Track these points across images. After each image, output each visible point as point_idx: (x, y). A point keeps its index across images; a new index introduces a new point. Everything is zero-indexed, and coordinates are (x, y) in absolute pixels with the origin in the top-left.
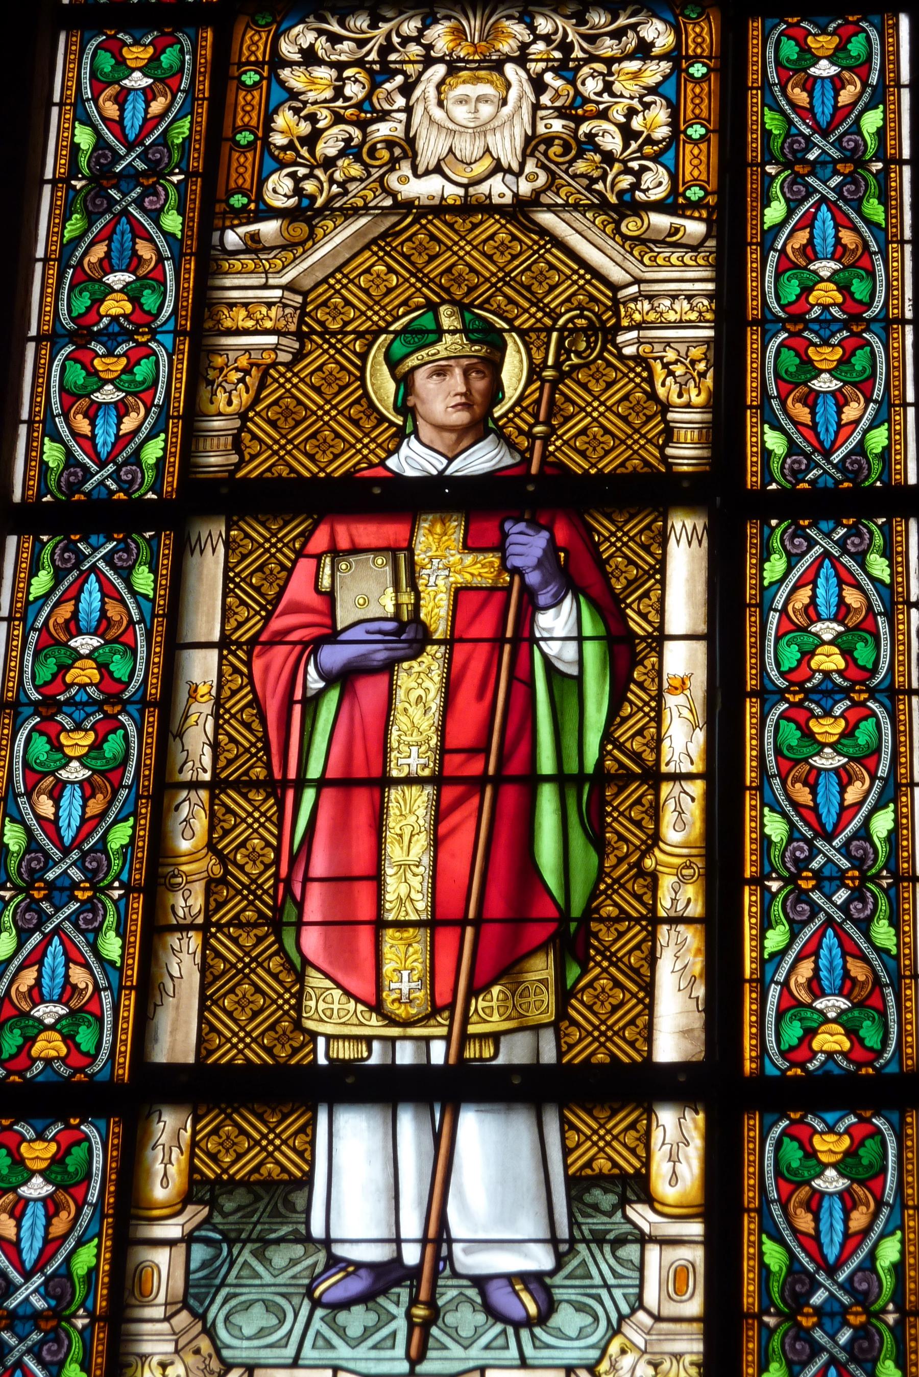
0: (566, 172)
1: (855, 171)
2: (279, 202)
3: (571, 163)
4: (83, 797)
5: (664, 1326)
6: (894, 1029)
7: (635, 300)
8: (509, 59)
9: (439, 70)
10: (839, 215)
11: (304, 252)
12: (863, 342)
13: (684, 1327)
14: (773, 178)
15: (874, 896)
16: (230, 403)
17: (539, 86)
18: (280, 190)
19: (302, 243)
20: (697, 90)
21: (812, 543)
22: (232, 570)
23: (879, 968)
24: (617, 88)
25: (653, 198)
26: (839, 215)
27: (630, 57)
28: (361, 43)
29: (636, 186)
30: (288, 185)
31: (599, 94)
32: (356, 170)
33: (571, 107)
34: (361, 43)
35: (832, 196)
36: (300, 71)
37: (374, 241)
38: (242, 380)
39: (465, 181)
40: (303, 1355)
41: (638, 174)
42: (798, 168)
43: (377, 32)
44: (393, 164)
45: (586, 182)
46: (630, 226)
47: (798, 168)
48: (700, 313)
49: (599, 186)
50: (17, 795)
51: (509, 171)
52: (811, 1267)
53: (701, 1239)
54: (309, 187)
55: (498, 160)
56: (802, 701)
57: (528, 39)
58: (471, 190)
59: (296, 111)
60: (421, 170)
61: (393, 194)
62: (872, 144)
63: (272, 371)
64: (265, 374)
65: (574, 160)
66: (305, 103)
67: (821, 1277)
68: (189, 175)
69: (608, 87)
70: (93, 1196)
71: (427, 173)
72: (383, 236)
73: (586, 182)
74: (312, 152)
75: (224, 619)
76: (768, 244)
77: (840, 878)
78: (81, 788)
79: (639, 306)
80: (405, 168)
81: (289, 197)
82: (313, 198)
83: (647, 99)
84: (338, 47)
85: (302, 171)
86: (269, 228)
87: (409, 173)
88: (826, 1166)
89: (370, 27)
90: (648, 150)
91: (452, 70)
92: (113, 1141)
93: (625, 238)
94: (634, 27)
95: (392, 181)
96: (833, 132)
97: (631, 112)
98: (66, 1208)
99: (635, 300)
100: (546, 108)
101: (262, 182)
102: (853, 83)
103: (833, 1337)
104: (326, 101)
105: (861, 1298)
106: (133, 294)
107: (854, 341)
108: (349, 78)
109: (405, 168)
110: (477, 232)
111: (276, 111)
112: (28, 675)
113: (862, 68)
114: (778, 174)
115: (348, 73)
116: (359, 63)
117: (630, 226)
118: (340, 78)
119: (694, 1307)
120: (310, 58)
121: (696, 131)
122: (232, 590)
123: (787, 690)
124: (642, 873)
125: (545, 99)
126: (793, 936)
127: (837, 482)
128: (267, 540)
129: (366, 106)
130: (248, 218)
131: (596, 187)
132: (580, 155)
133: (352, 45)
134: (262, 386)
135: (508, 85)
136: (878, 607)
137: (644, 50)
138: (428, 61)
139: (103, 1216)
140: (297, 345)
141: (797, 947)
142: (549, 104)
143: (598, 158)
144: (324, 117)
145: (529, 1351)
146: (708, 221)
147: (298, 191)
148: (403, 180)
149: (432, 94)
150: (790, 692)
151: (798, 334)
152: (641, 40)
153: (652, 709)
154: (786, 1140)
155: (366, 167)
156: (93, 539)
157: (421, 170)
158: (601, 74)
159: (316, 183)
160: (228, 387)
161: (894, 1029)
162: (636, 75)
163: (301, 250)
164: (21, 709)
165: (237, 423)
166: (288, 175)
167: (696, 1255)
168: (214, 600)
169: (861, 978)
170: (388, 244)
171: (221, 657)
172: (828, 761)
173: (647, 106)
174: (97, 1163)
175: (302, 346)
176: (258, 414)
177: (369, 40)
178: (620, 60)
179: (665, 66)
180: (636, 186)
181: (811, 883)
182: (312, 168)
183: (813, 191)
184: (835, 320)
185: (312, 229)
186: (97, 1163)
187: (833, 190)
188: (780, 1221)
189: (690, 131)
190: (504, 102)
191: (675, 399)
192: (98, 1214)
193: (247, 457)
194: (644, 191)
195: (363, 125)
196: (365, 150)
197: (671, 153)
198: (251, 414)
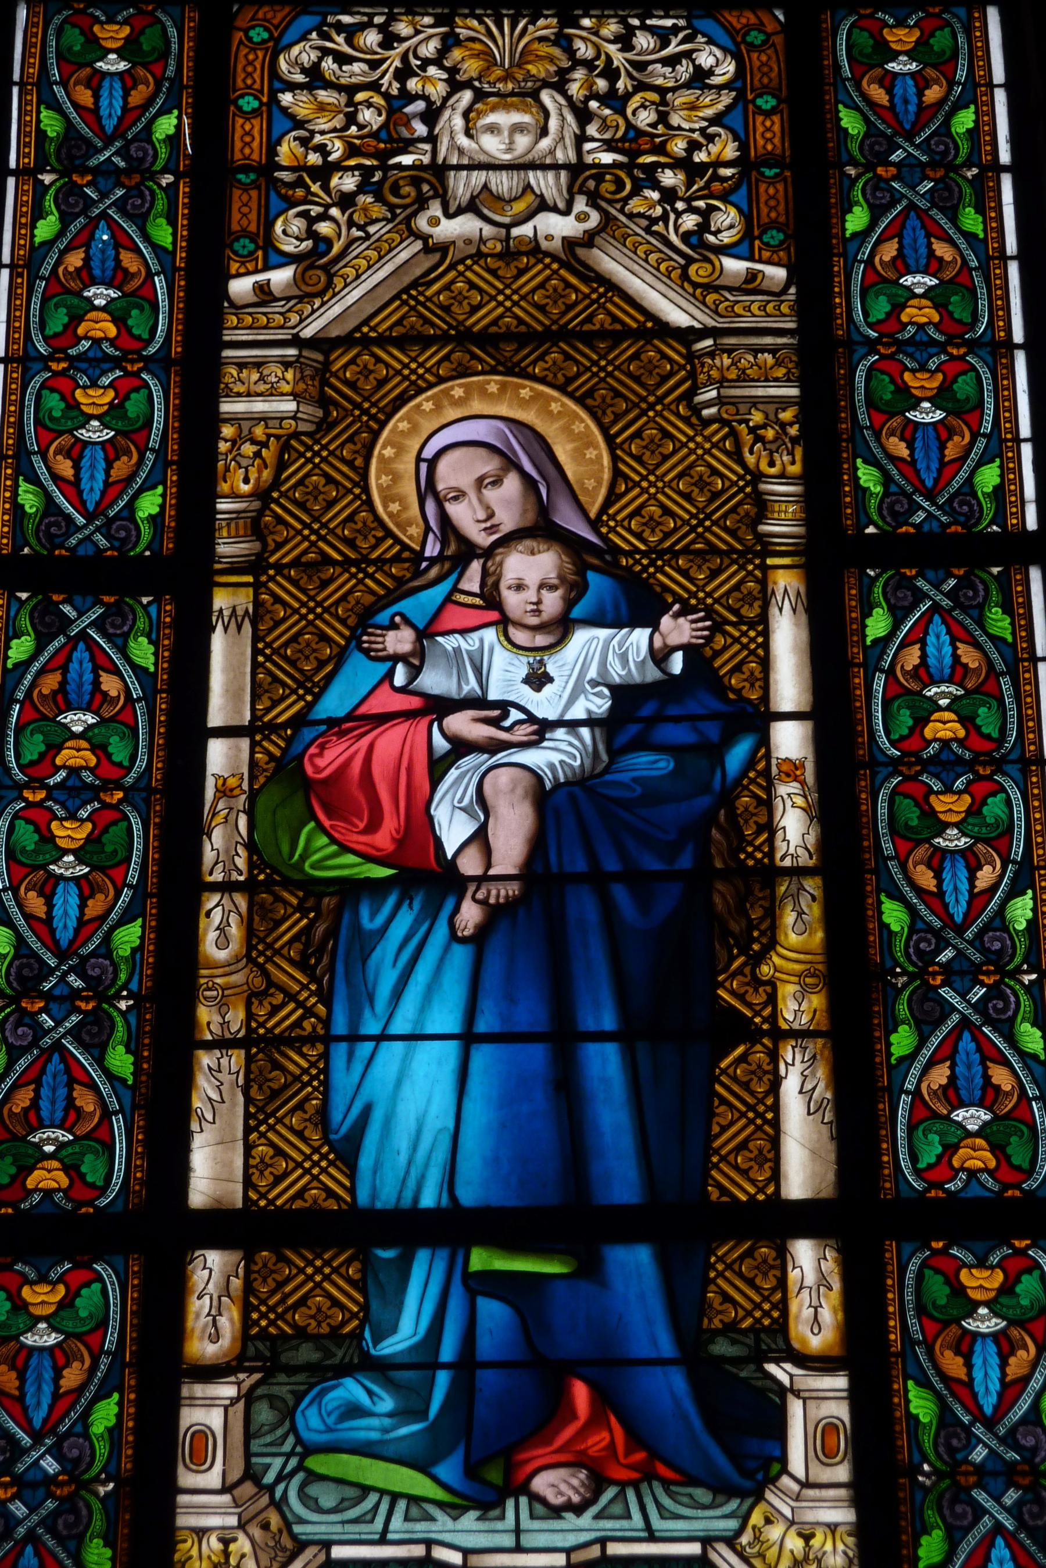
0: (622, 211)
1: (946, 175)
2: (289, 246)
3: (625, 200)
4: (106, 459)
5: (811, 1493)
6: (1013, 713)
7: (712, 355)
8: (546, 84)
9: (467, 96)
10: (956, 628)
11: (323, 304)
12: (966, 367)
13: (832, 1493)
14: (854, 181)
15: (983, 582)
16: (246, 481)
17: (583, 116)
18: (289, 231)
19: (321, 294)
20: (771, 191)
21: (922, 596)
22: (262, 639)
23: (995, 656)
24: (675, 120)
25: (726, 241)
26: (956, 628)
27: (688, 85)
28: (374, 65)
29: (704, 227)
30: (297, 226)
31: (653, 125)
32: (378, 211)
33: (623, 139)
34: (374, 65)
35: (946, 603)
36: (304, 96)
37: (406, 290)
38: (258, 454)
39: (507, 220)
40: (391, 1527)
41: (706, 214)
42: (880, 170)
43: (392, 52)
44: (421, 203)
45: (644, 223)
46: (698, 272)
47: (880, 170)
48: (769, 35)
49: (659, 228)
50: (30, 453)
51: (555, 209)
52: (966, 1419)
53: (844, 1394)
54: (324, 228)
55: (542, 196)
56: (893, 354)
57: (566, 64)
58: (516, 232)
59: (304, 142)
60: (452, 209)
61: (425, 238)
62: (964, 148)
63: (293, 442)
64: (286, 447)
65: (630, 196)
66: (312, 133)
67: (979, 1430)
68: (178, 176)
69: (663, 118)
70: (154, 440)
71: (460, 211)
72: (415, 284)
73: (644, 223)
74: (326, 188)
75: (255, 698)
76: (872, 662)
77: (974, 973)
78: (104, 449)
79: (717, 362)
80: (435, 209)
81: (302, 240)
82: (328, 242)
83: (712, 130)
84: (344, 68)
85: (315, 210)
86: (281, 277)
87: (439, 213)
88: (978, 1304)
89: (380, 45)
90: (716, 186)
91: (480, 95)
92: (174, 390)
93: (695, 285)
94: (688, 54)
95: (422, 223)
96: (918, 134)
97: (693, 146)
98: (128, 453)
99: (712, 355)
100: (593, 140)
101: (270, 225)
102: (937, 82)
103: (960, 953)
104: (334, 130)
105: (992, 957)
106: (117, 314)
107: (954, 367)
108: (360, 103)
109: (435, 209)
110: (523, 279)
111: (279, 143)
112: (34, 320)
113: (945, 64)
114: (859, 176)
115: (360, 97)
116: (374, 86)
117: (701, 272)
118: (350, 103)
119: (842, 1473)
120: (315, 78)
121: (767, 102)
122: (262, 665)
123: (878, 341)
124: (757, 982)
125: (592, 130)
126: (922, 1041)
127: (944, 526)
128: (303, 604)
129: (383, 135)
130: (253, 1116)
131: (655, 228)
132: (636, 191)
133: (364, 67)
134: (281, 466)
135: (547, 114)
136: (1000, 665)
137: (700, 77)
138: (455, 86)
139: (167, 464)
140: (320, 413)
141: (927, 1053)
142: (597, 136)
143: (655, 195)
144: (337, 150)
145: (657, 1523)
146: (788, 267)
147: (311, 234)
148: (434, 222)
149: (458, 122)
150: (904, 764)
151: (914, 778)
152: (698, 68)
153: (774, 1306)
154: (928, 1272)
155: (392, 208)
156: (90, 550)
157: (452, 209)
158: (653, 103)
159: (334, 226)
160: (244, 462)
161: (1013, 713)
162: (693, 107)
163: (317, 303)
164: (29, 364)
165: (256, 505)
166: (299, 215)
167: (841, 1411)
168: (243, 702)
169: (973, 665)
170: (421, 293)
171: (253, 745)
172: (953, 840)
173: (711, 138)
174: (158, 417)
175: (327, 413)
176: (283, 495)
177: (383, 61)
178: (673, 90)
179: (726, 99)
180: (704, 227)
181: (972, 1479)
182: (327, 207)
183: (922, 596)
184: (933, 342)
185: (330, 277)
186: (158, 417)
187: (947, 595)
188: (898, 877)
189: (759, 102)
190: (544, 132)
191: (764, 466)
192: (159, 465)
193: (272, 545)
194: (715, 234)
195: (383, 156)
196: (387, 185)
197: (744, 190)
198: (275, 495)
